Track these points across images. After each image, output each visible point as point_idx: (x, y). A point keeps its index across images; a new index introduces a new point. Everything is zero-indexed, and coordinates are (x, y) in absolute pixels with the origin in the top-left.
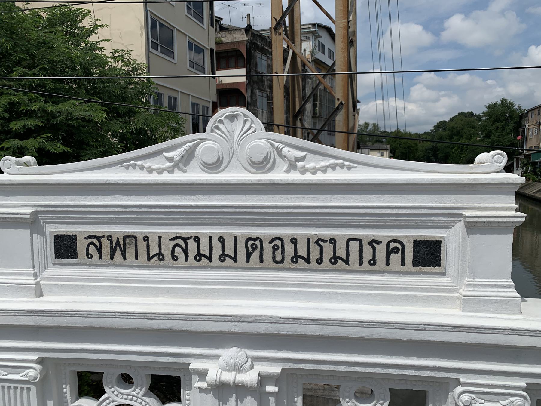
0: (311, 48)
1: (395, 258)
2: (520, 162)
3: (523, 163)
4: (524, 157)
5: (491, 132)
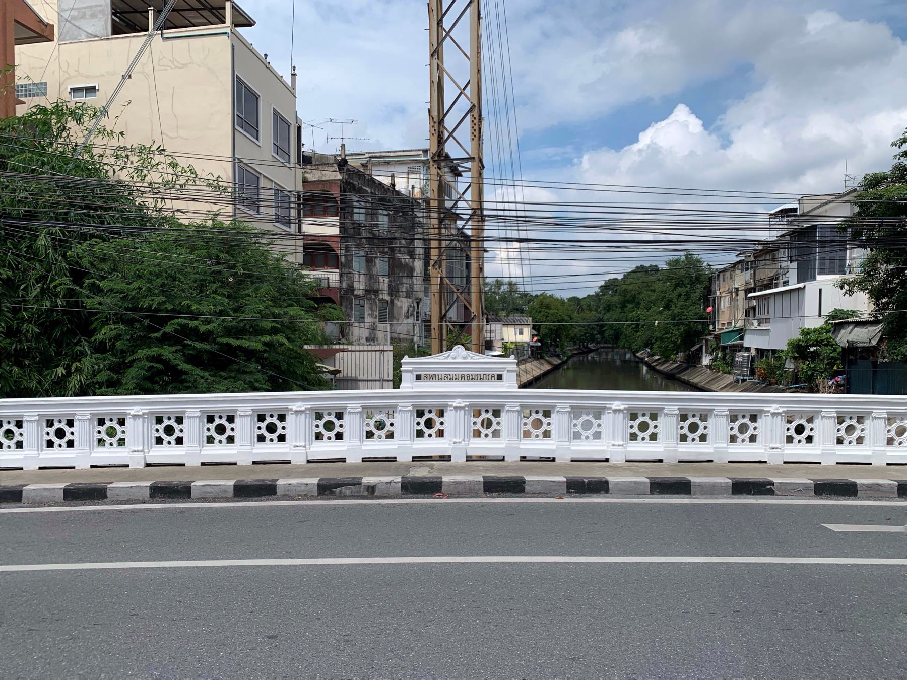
0: (422, 184)
1: (493, 378)
5: (671, 301)
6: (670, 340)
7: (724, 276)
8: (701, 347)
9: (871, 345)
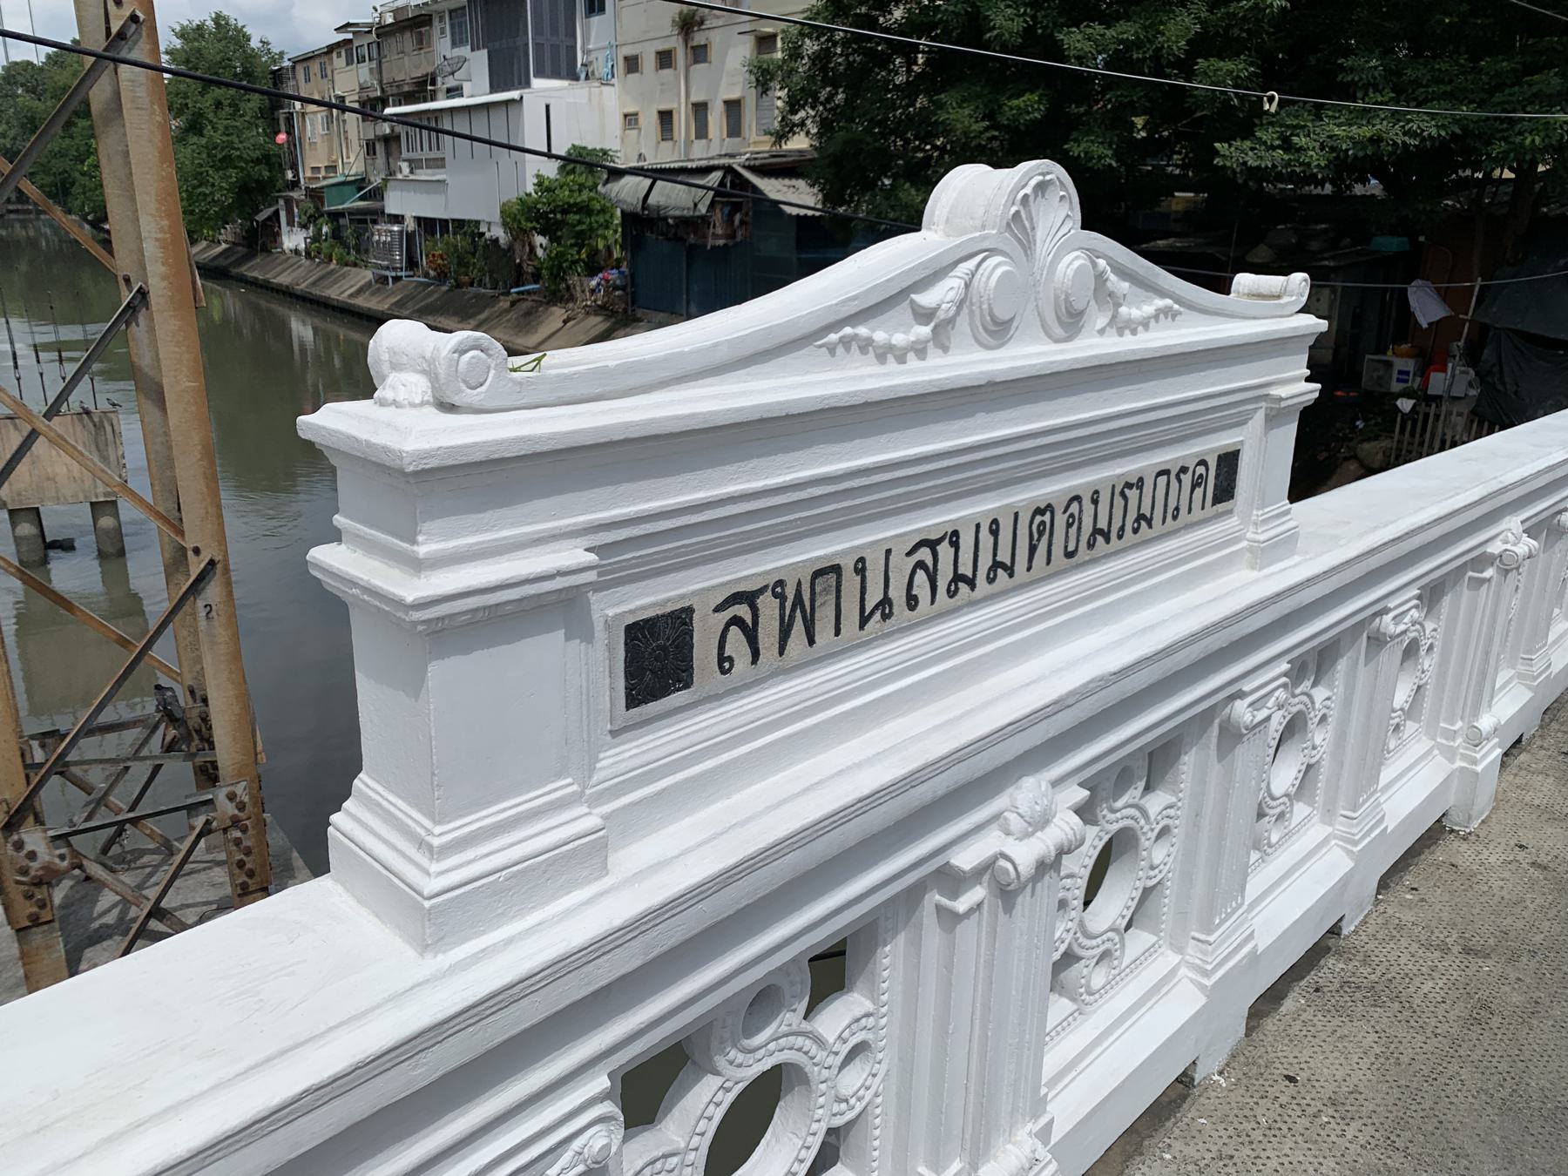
2: (296, 210)
3: (305, 214)
4: (306, 195)
6: (209, 199)
7: (307, 71)
8: (277, 213)
9: (697, 214)
